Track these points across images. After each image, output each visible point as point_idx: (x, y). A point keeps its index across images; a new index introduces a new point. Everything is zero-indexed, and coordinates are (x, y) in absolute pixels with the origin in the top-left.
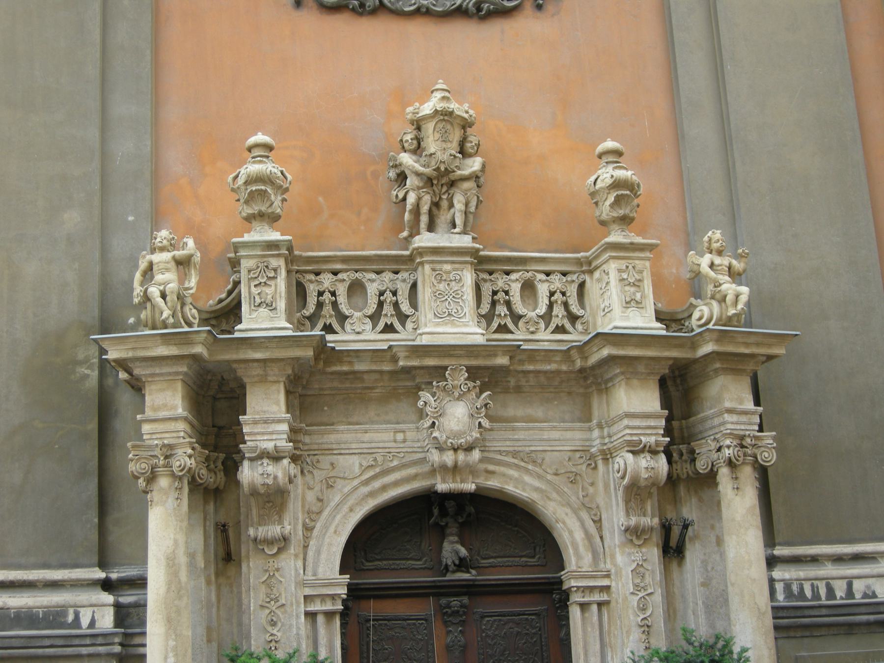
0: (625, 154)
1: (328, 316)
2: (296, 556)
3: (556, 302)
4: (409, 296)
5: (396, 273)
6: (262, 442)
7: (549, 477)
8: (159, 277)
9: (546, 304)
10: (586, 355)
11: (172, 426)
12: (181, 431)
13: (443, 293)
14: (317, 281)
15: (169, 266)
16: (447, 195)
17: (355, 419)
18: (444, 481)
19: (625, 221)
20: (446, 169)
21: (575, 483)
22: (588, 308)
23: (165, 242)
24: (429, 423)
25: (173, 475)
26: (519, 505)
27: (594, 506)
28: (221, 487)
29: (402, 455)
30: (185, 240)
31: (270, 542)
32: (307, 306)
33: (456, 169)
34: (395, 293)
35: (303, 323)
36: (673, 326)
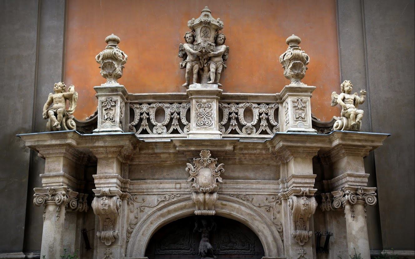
0: (301, 42)
1: (144, 125)
2: (121, 246)
3: (232, 117)
4: (155, 116)
5: (180, 103)
6: (104, 188)
7: (255, 208)
8: (55, 105)
9: (257, 119)
10: (274, 145)
11: (57, 179)
12: (61, 182)
13: (201, 114)
14: (140, 108)
15: (61, 100)
16: (207, 64)
17: (156, 177)
18: (199, 209)
19: (299, 77)
20: (206, 51)
21: (269, 211)
22: (279, 122)
23: (59, 88)
24: (191, 179)
25: (56, 205)
26: (241, 222)
27: (279, 224)
28: (86, 211)
29: (179, 195)
30: (70, 87)
31: (107, 239)
32: (134, 120)
33: (211, 51)
34: (179, 114)
35: (132, 128)
36: (325, 131)
